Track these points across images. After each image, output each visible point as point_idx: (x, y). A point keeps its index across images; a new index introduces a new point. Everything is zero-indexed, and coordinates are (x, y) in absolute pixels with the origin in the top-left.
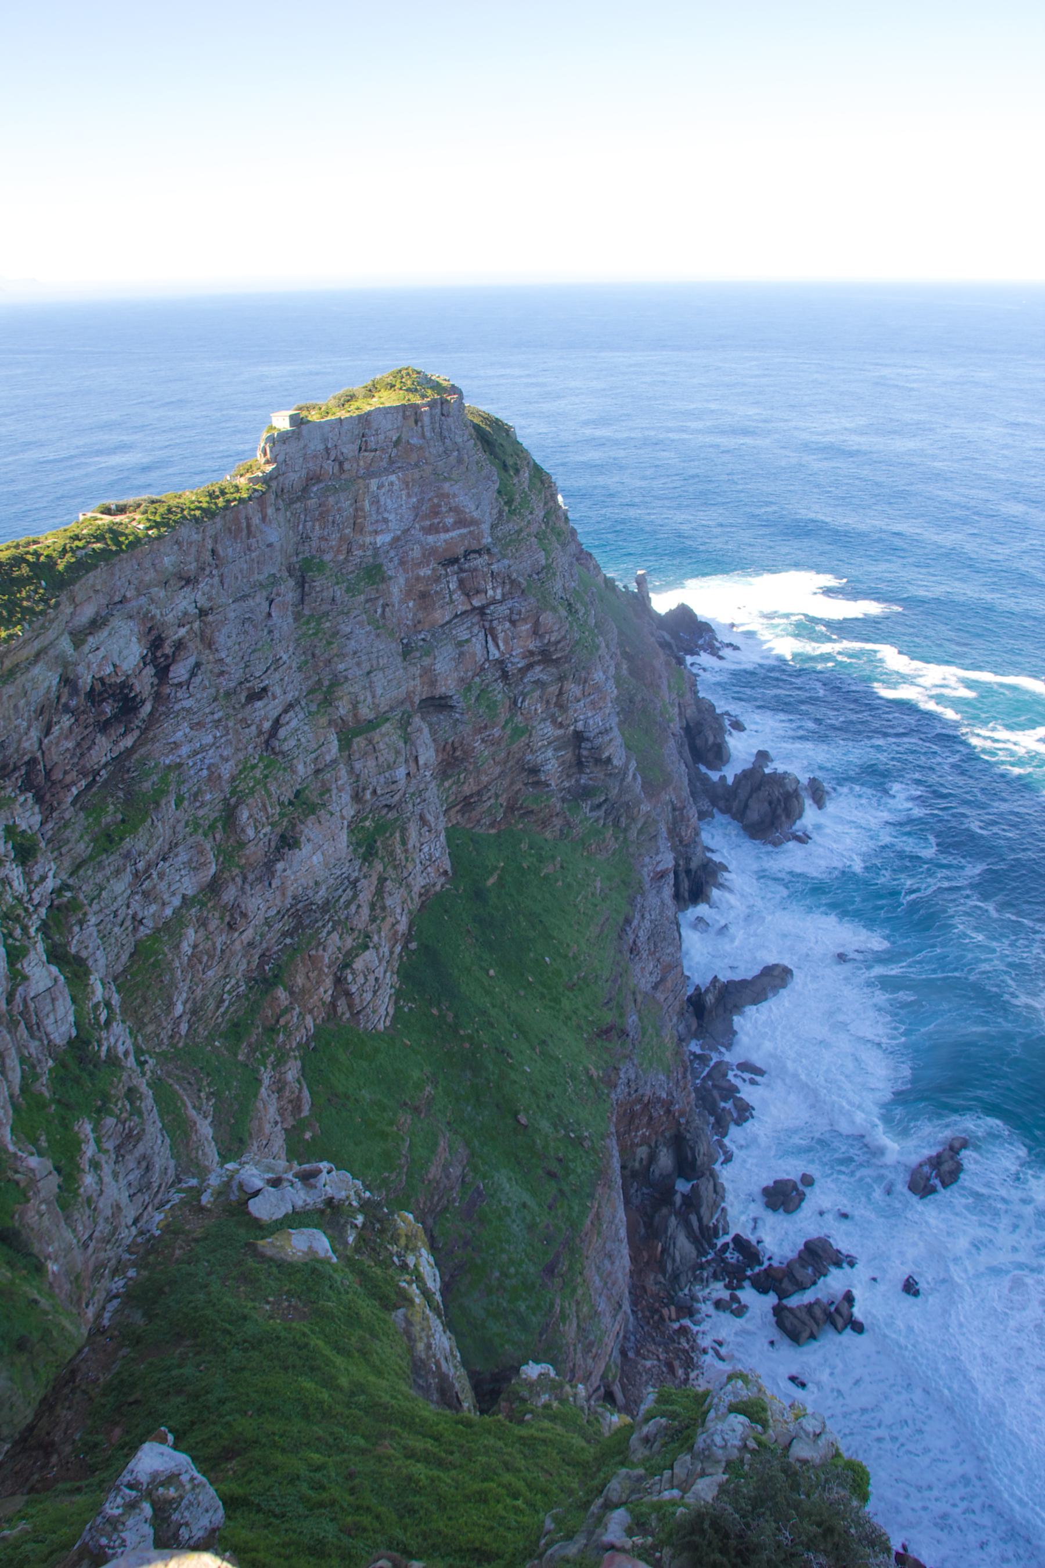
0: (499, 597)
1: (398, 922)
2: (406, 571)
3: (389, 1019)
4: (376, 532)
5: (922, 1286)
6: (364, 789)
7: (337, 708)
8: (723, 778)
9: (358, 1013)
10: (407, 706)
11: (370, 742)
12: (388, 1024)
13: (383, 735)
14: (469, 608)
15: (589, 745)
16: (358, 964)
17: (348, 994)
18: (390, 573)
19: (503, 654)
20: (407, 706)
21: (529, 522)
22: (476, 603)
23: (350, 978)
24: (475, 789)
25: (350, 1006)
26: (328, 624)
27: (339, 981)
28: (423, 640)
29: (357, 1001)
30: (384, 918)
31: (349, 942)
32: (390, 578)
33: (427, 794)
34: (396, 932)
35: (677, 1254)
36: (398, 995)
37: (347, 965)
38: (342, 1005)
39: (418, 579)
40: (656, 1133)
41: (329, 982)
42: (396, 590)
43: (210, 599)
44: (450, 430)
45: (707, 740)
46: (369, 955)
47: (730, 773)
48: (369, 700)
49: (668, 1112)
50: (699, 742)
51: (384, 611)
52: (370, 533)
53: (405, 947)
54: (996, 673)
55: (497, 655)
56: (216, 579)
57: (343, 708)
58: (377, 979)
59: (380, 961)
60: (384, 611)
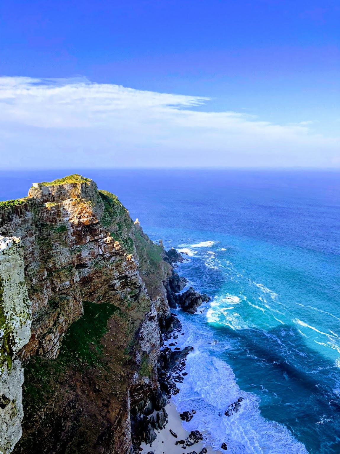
0: (102, 237)
1: (63, 327)
2: (73, 228)
3: (57, 355)
4: (64, 217)
5: (228, 447)
6: (56, 288)
7: (49, 264)
8: (179, 295)
9: (46, 353)
10: (72, 265)
11: (59, 274)
12: (56, 357)
13: (63, 273)
14: (94, 240)
15: (129, 279)
16: (47, 338)
17: (43, 347)
18: (68, 228)
19: (103, 252)
20: (72, 265)
21: (116, 219)
22: (96, 238)
23: (44, 342)
24: (93, 290)
25: (44, 351)
26: (47, 241)
27: (40, 344)
28: (78, 247)
29: (46, 349)
30: (58, 326)
31: (45, 331)
32: (68, 230)
33: (77, 290)
34: (63, 330)
35: (150, 436)
36: (61, 349)
37: (44, 338)
38: (41, 350)
39: (77, 230)
40: (146, 396)
41: (37, 343)
42: (70, 233)
43: (6, 230)
44: (88, 191)
45: (175, 284)
46: (52, 335)
47: (181, 292)
48: (59, 262)
49: (149, 389)
50: (173, 285)
51: (65, 239)
52: (63, 217)
53: (65, 335)
54: (335, 333)
55: (102, 253)
56: (9, 225)
57: (51, 265)
58: (54, 343)
59: (55, 338)
60: (65, 239)
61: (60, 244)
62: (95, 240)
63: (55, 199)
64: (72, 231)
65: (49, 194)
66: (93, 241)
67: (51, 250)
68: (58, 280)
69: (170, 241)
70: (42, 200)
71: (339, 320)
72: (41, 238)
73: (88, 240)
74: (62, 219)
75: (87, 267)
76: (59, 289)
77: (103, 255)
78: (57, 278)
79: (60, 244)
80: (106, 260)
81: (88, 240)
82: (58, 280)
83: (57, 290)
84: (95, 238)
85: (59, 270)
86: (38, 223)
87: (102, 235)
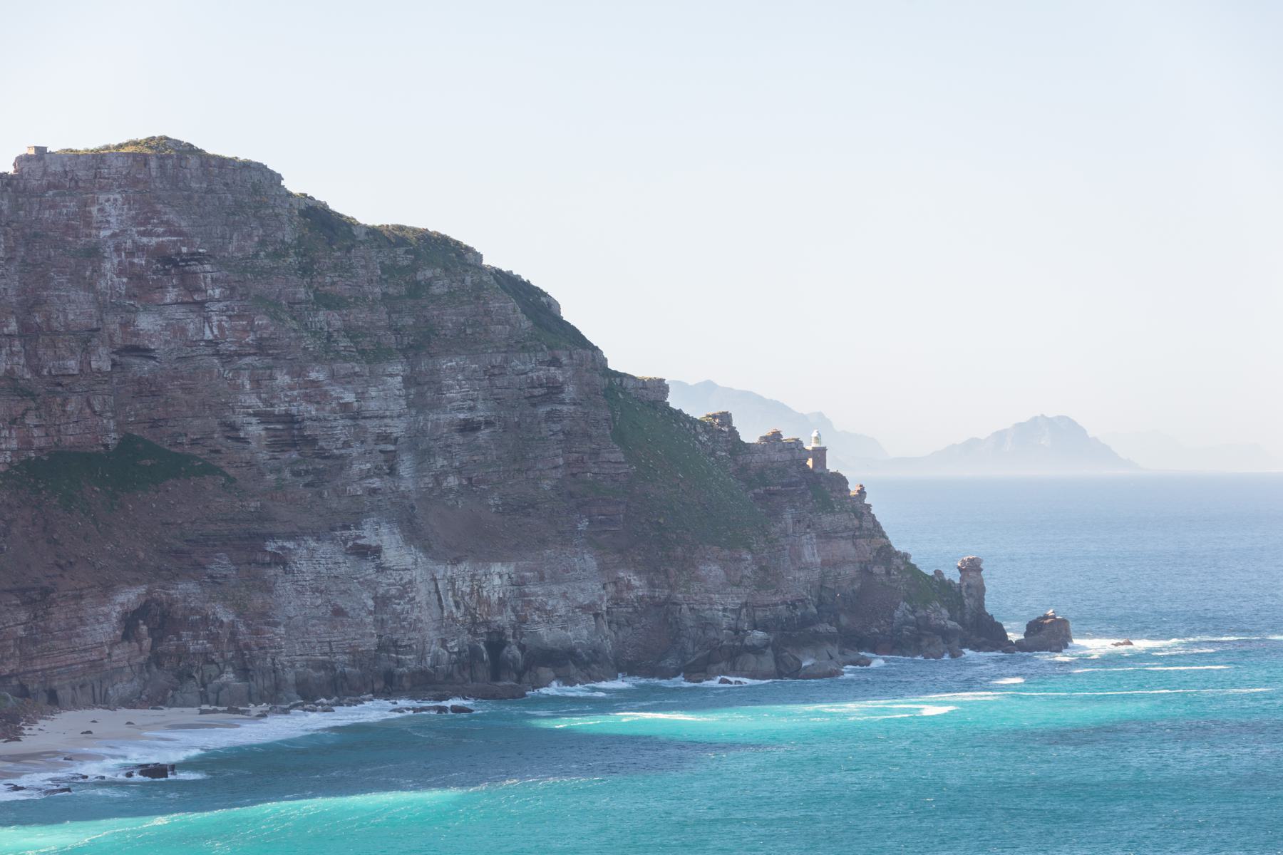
2: (120, 256)
6: (42, 367)
15: (297, 426)
39: (132, 264)
55: (211, 337)
61: (70, 281)
62: (196, 303)
63: (81, 184)
64: (116, 261)
65: (66, 172)
66: (187, 303)
67: (46, 289)
68: (50, 353)
69: (565, 408)
70: (44, 182)
71: (1011, 630)
72: (29, 261)
73: (171, 296)
74: (94, 232)
75: (154, 358)
76: (50, 372)
77: (217, 344)
78: (47, 346)
79: (70, 281)
80: (227, 358)
81: (171, 296)
82: (50, 353)
83: (45, 372)
84: (195, 297)
85: (57, 333)
86: (27, 231)
87: (218, 291)
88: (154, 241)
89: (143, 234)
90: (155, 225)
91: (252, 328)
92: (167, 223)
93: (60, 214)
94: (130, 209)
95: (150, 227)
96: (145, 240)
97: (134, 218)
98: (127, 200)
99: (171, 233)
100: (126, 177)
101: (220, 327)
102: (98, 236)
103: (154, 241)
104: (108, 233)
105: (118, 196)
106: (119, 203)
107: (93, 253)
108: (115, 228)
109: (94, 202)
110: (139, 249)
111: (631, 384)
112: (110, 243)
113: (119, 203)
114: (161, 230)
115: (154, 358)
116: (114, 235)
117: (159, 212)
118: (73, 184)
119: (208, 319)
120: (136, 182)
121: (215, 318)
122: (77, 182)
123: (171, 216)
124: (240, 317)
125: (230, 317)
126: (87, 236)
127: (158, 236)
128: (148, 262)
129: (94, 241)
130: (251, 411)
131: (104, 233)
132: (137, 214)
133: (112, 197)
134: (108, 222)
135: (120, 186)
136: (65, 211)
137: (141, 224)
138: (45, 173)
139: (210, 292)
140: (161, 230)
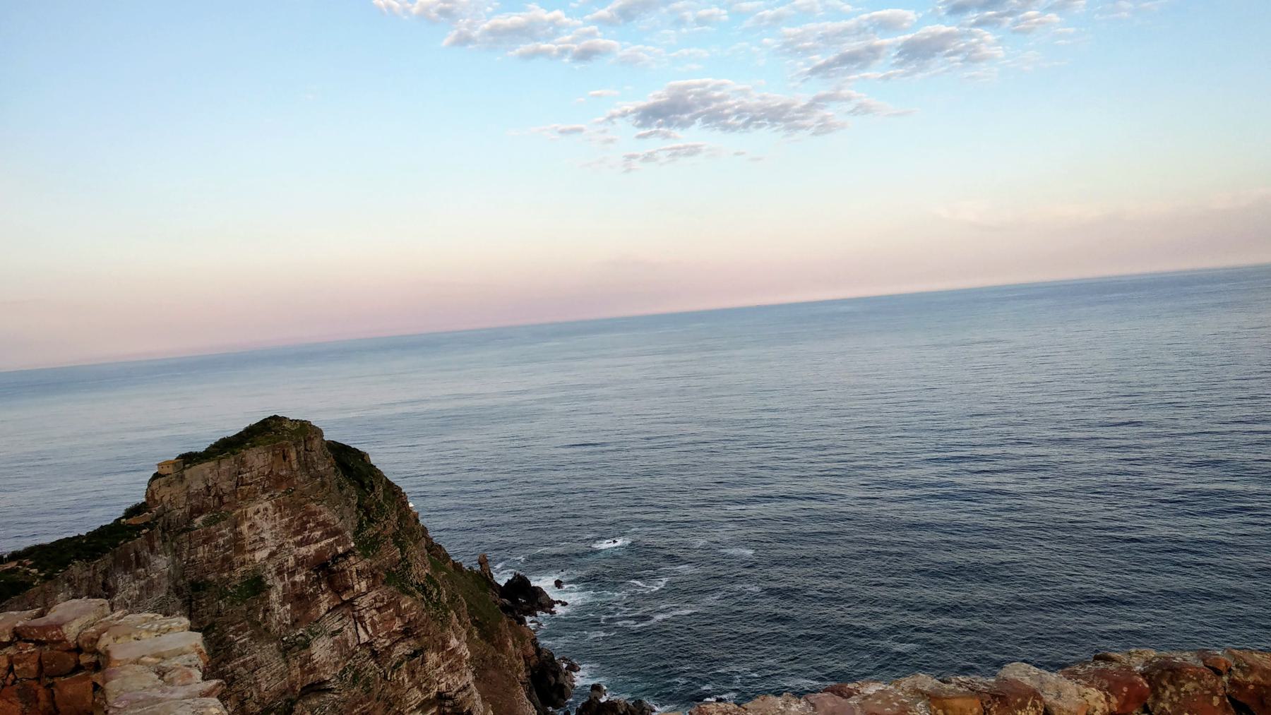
2: (282, 579)
39: (294, 584)
55: (367, 638)
70: (187, 509)
75: (330, 690)
79: (252, 637)
87: (363, 584)
88: (313, 548)
89: (299, 544)
90: (312, 530)
91: (399, 613)
92: (324, 524)
93: (216, 547)
94: (282, 517)
95: (306, 533)
96: (303, 550)
97: (287, 527)
98: (278, 507)
99: (328, 534)
100: (268, 477)
101: (373, 625)
102: (253, 561)
103: (313, 548)
104: (263, 554)
105: (267, 504)
106: (270, 512)
107: (256, 586)
108: (271, 545)
109: (244, 517)
110: (300, 562)
111: (287, 425)
112: (270, 566)
113: (270, 512)
114: (318, 534)
115: (330, 690)
116: (272, 555)
117: (315, 513)
118: (216, 500)
119: (360, 619)
120: (279, 481)
121: (367, 616)
122: (221, 498)
123: (326, 515)
124: (387, 606)
125: (378, 609)
126: (242, 564)
127: (317, 542)
128: (307, 575)
129: (250, 567)
130: (1161, 495)
131: (261, 555)
132: (291, 521)
133: (261, 507)
134: (262, 540)
135: (264, 491)
136: (221, 541)
137: (297, 533)
138: (189, 496)
139: (357, 587)
140: (318, 534)
